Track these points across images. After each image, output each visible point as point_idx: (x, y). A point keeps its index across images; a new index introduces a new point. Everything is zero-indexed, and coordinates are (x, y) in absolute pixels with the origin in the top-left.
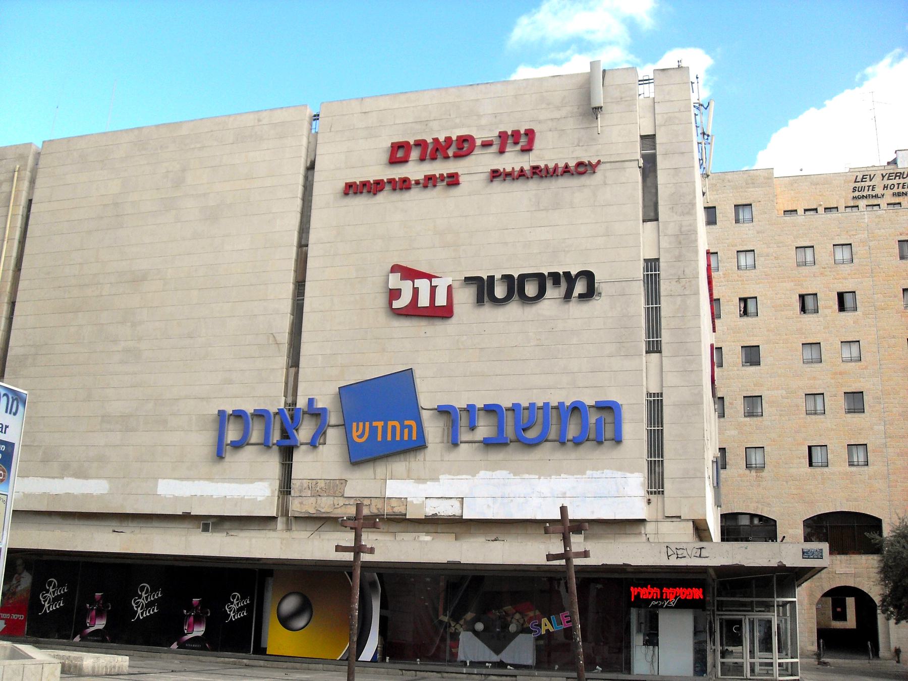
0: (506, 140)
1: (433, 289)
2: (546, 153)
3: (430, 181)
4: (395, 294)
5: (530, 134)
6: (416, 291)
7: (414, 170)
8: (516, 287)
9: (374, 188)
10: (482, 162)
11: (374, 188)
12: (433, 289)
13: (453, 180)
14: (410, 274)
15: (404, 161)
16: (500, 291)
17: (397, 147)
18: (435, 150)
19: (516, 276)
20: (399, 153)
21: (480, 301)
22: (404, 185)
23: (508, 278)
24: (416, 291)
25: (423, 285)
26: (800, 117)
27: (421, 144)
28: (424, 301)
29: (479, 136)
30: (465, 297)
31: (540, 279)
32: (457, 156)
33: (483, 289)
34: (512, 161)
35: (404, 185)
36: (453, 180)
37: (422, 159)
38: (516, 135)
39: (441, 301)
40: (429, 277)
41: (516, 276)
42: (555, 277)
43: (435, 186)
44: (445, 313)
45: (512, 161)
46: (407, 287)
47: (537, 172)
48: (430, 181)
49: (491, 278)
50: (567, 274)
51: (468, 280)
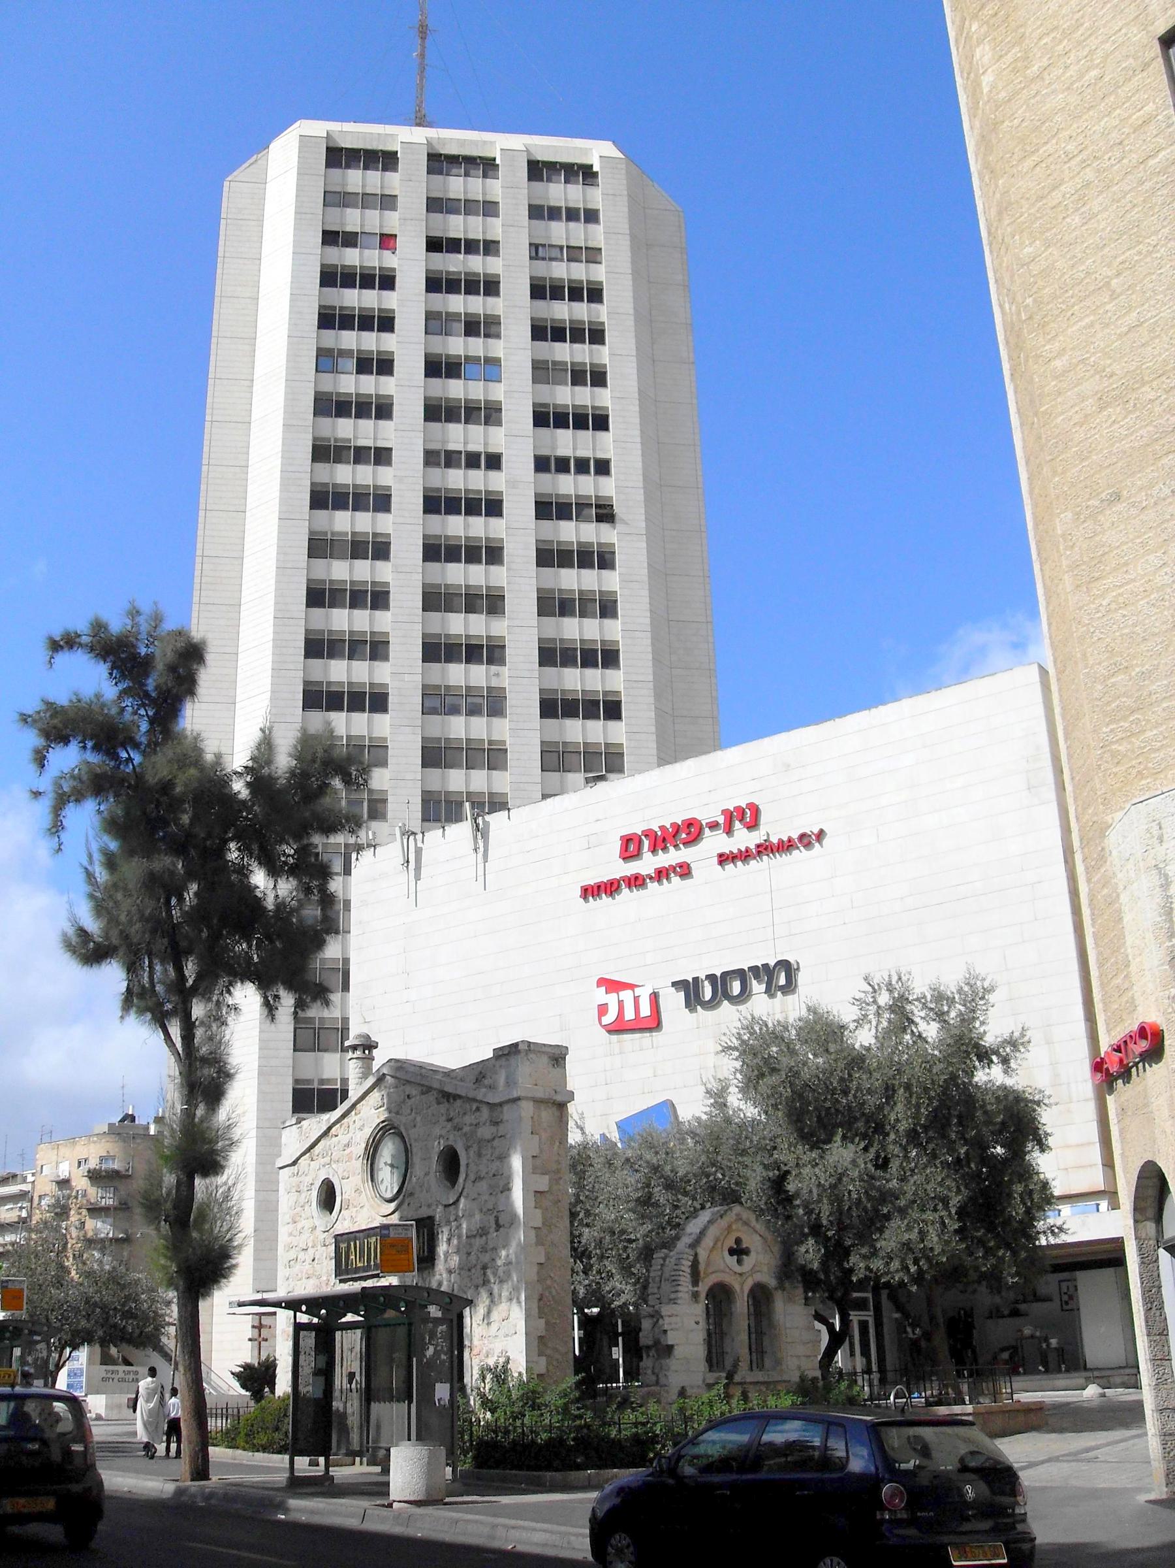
0: (732, 818)
1: (636, 1000)
2: (773, 828)
3: (661, 874)
4: (603, 1010)
5: (755, 810)
6: (621, 1004)
7: (648, 864)
8: (720, 983)
9: (610, 888)
10: (714, 843)
11: (610, 888)
12: (636, 1000)
13: (684, 871)
14: (612, 986)
15: (637, 855)
16: (708, 993)
17: (627, 840)
18: (660, 840)
19: (719, 975)
20: (630, 847)
21: (688, 1005)
22: (636, 882)
23: (711, 978)
24: (621, 1004)
25: (627, 996)
26: (874, 710)
27: (648, 833)
28: (629, 1015)
29: (704, 817)
30: (672, 1002)
31: (741, 974)
32: (687, 843)
33: (690, 991)
34: (743, 839)
35: (636, 882)
36: (684, 871)
37: (653, 850)
38: (741, 811)
39: (645, 1011)
40: (632, 987)
41: (719, 975)
42: (755, 970)
43: (224, 1023)
44: (654, 1023)
45: (743, 839)
46: (612, 1000)
47: (765, 849)
48: (661, 874)
49: (696, 979)
50: (766, 966)
51: (674, 984)
